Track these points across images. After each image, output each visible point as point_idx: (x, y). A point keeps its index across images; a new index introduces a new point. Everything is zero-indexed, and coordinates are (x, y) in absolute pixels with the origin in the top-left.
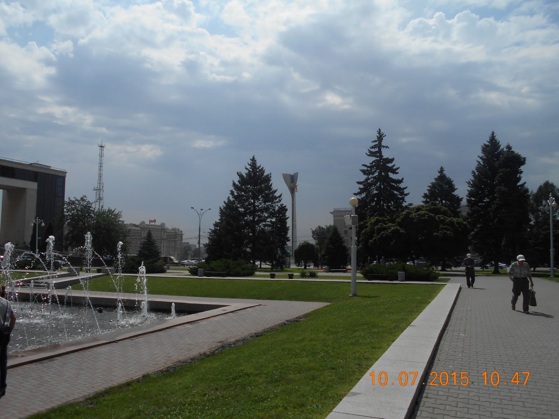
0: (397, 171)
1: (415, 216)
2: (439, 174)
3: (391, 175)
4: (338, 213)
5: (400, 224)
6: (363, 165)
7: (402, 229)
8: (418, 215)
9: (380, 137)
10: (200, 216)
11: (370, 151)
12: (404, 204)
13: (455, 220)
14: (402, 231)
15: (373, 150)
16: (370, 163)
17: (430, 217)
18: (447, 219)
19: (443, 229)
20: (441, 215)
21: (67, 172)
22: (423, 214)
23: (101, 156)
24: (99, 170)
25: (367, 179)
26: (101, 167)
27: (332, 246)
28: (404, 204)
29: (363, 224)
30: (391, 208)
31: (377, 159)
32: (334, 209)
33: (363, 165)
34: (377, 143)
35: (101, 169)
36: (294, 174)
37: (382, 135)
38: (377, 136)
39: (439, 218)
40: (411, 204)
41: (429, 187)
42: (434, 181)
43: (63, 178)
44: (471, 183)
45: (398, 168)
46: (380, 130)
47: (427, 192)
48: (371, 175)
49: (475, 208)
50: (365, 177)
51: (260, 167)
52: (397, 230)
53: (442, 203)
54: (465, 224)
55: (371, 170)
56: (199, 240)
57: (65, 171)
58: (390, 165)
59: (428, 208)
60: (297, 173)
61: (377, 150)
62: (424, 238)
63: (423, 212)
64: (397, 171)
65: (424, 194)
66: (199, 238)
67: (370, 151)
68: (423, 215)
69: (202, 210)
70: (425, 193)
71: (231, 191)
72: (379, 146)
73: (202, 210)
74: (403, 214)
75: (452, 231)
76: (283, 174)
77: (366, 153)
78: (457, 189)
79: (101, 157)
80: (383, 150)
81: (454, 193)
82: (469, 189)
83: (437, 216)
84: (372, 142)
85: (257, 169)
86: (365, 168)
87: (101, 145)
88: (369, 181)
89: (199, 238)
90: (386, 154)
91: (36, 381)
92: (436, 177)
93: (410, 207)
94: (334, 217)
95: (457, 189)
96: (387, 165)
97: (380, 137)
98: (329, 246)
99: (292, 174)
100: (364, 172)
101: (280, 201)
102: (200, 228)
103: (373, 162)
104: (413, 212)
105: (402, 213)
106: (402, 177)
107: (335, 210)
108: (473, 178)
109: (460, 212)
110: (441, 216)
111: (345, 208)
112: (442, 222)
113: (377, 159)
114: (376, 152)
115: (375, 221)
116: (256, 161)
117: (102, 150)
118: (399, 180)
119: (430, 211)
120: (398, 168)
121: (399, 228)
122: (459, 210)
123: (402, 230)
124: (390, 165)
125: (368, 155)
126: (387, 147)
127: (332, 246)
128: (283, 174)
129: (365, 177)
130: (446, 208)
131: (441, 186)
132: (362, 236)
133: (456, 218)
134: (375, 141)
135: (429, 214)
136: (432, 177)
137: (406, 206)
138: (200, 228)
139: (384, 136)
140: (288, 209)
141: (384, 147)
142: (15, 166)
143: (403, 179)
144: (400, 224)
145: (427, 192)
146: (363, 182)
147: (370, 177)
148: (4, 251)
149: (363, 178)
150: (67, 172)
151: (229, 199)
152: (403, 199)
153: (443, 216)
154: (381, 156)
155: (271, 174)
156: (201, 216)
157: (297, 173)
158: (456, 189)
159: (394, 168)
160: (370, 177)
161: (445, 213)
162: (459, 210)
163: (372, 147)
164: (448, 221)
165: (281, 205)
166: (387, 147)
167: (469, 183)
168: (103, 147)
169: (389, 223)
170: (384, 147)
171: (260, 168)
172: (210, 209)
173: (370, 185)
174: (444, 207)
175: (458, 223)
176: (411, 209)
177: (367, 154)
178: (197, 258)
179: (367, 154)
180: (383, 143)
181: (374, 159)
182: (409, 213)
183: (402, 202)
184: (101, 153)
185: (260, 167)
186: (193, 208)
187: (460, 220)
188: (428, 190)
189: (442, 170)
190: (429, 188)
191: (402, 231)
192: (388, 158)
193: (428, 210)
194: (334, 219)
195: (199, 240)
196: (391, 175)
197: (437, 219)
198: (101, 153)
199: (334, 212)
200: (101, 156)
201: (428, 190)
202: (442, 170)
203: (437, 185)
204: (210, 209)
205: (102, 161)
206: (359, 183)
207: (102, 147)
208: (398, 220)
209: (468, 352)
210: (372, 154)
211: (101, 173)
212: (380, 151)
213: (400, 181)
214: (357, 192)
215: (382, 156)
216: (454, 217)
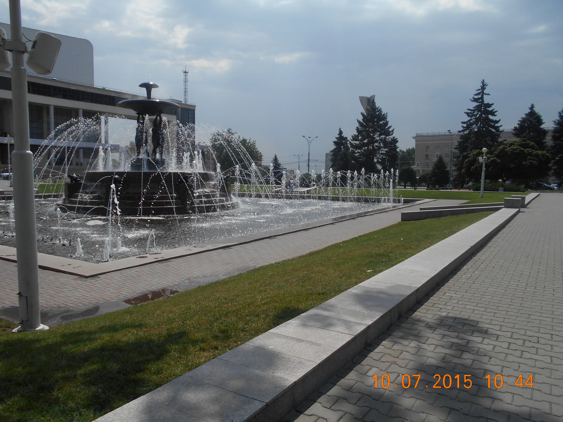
0: (495, 114)
1: (509, 150)
2: (529, 111)
3: (491, 117)
4: (420, 138)
5: (497, 156)
6: (468, 109)
7: (498, 159)
8: (512, 149)
9: (483, 87)
10: (309, 143)
11: (474, 98)
12: (500, 140)
13: (540, 152)
14: (499, 161)
15: (476, 97)
16: (474, 107)
17: (522, 150)
18: (534, 152)
19: (530, 159)
20: (529, 148)
21: (196, 106)
22: (515, 149)
23: (186, 81)
24: (184, 95)
25: (469, 121)
26: (186, 92)
27: (437, 171)
28: (500, 140)
29: (466, 155)
30: (488, 141)
31: (479, 104)
32: (416, 134)
33: (468, 109)
34: (480, 91)
35: (186, 95)
36: (371, 97)
37: (485, 85)
38: (481, 86)
39: (528, 151)
40: (505, 140)
41: (519, 121)
42: (524, 116)
43: (194, 111)
44: (557, 122)
45: (496, 111)
46: (483, 81)
47: (517, 126)
48: (473, 117)
49: (558, 142)
50: (469, 118)
51: (379, 108)
52: (495, 160)
53: (530, 135)
54: (548, 156)
55: (474, 113)
56: (309, 163)
57: (194, 105)
58: (490, 109)
59: (520, 144)
60: (374, 96)
61: (480, 96)
62: (515, 166)
63: (516, 147)
64: (495, 114)
65: (515, 127)
66: (309, 162)
67: (474, 98)
68: (516, 150)
69: (310, 137)
70: (516, 126)
71: (357, 127)
72: (482, 93)
73: (310, 137)
74: (500, 148)
75: (536, 161)
76: (359, 97)
77: (470, 99)
78: (544, 123)
79: (186, 82)
80: (485, 96)
81: (542, 126)
82: (555, 126)
83: (526, 150)
84: (476, 90)
85: (375, 109)
86: (470, 112)
87: (185, 71)
88: (471, 122)
89: (309, 162)
90: (487, 100)
91: (43, 305)
92: (527, 113)
93: (505, 142)
94: (416, 142)
95: (544, 123)
96: (487, 109)
97: (483, 87)
98: (436, 171)
99: (369, 96)
100: (468, 114)
101: (392, 134)
102: (309, 153)
103: (476, 106)
104: (507, 147)
105: (499, 147)
106: (502, 125)
107: (417, 135)
108: (558, 118)
109: (545, 142)
110: (529, 150)
111: (428, 133)
112: (530, 154)
113: (479, 104)
114: (479, 99)
115: (477, 153)
116: (375, 103)
117: (186, 76)
118: (497, 121)
119: (521, 145)
120: (496, 111)
121: (496, 158)
122: (544, 141)
123: (498, 160)
124: (490, 109)
125: (472, 101)
126: (488, 94)
127: (437, 171)
128: (359, 97)
129: (469, 118)
130: (533, 143)
131: (531, 121)
132: (465, 164)
133: (541, 151)
134: (479, 90)
135: (520, 148)
136: (522, 112)
137: (501, 141)
138: (309, 153)
139: (486, 86)
140: (399, 141)
141: (486, 94)
142: (113, 95)
143: (500, 120)
144: (497, 156)
145: (517, 126)
146: (466, 122)
147: (472, 118)
148: (103, 169)
149: (466, 119)
150: (196, 106)
151: (340, 130)
152: (498, 135)
153: (530, 150)
154: (483, 101)
155: (387, 114)
156: (310, 143)
157: (374, 96)
158: (543, 123)
159: (494, 111)
160: (472, 118)
161: (532, 147)
162: (544, 141)
163: (476, 95)
164: (534, 153)
165: (393, 138)
166: (488, 94)
167: (555, 122)
168: (187, 72)
169: (488, 154)
170: (486, 94)
171: (379, 109)
172: (317, 137)
173: (472, 124)
174: (532, 143)
175: (542, 155)
176: (505, 144)
177: (471, 100)
178: (556, 184)
179: (471, 100)
180: (485, 92)
181: (476, 104)
182: (504, 148)
183: (498, 137)
184: (186, 79)
185: (379, 108)
186: (304, 136)
187: (544, 152)
188: (518, 124)
189: (532, 107)
190: (519, 123)
191: (499, 161)
192: (488, 103)
193: (519, 145)
194: (416, 144)
195: (309, 163)
196: (491, 117)
197: (526, 152)
198: (186, 79)
199: (417, 136)
200: (186, 81)
201: (518, 124)
202: (532, 107)
203: (527, 119)
204: (317, 137)
205: (186, 86)
206: (463, 123)
207: (185, 72)
208: (496, 152)
209: (542, 289)
210: (475, 100)
211: (186, 98)
212: (482, 98)
213: (497, 122)
214: (461, 130)
215: (484, 102)
216: (540, 150)
